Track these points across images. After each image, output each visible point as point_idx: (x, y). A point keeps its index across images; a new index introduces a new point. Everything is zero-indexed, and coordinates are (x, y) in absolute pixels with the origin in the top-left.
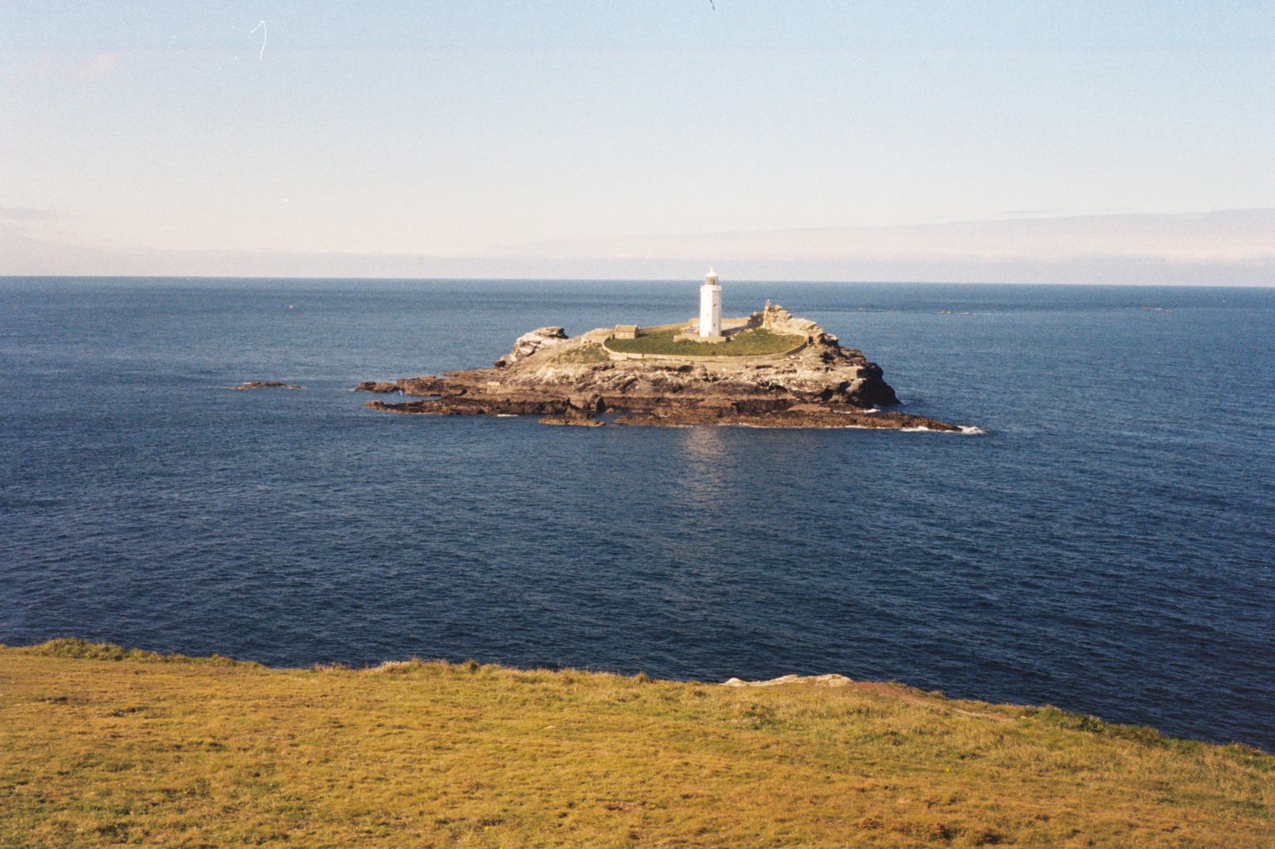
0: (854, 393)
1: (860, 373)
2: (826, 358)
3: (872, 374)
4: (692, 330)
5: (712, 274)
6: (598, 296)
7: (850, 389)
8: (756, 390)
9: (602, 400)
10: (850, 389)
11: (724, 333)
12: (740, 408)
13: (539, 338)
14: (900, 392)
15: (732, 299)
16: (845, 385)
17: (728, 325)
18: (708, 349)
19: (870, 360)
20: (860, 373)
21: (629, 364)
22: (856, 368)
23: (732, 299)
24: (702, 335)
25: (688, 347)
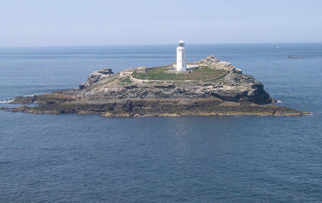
0: (251, 96)
1: (253, 87)
2: (236, 79)
3: (259, 88)
4: (174, 69)
5: (181, 42)
6: (56, 57)
7: (249, 94)
8: (204, 96)
9: (131, 102)
10: (249, 94)
11: (188, 70)
12: (196, 106)
13: (99, 74)
14: (272, 95)
15: (190, 53)
16: (246, 92)
17: (189, 66)
18: (181, 76)
19: (257, 82)
20: (253, 87)
21: (143, 85)
22: (251, 84)
23: (190, 53)
24: (178, 70)
25: (173, 76)
